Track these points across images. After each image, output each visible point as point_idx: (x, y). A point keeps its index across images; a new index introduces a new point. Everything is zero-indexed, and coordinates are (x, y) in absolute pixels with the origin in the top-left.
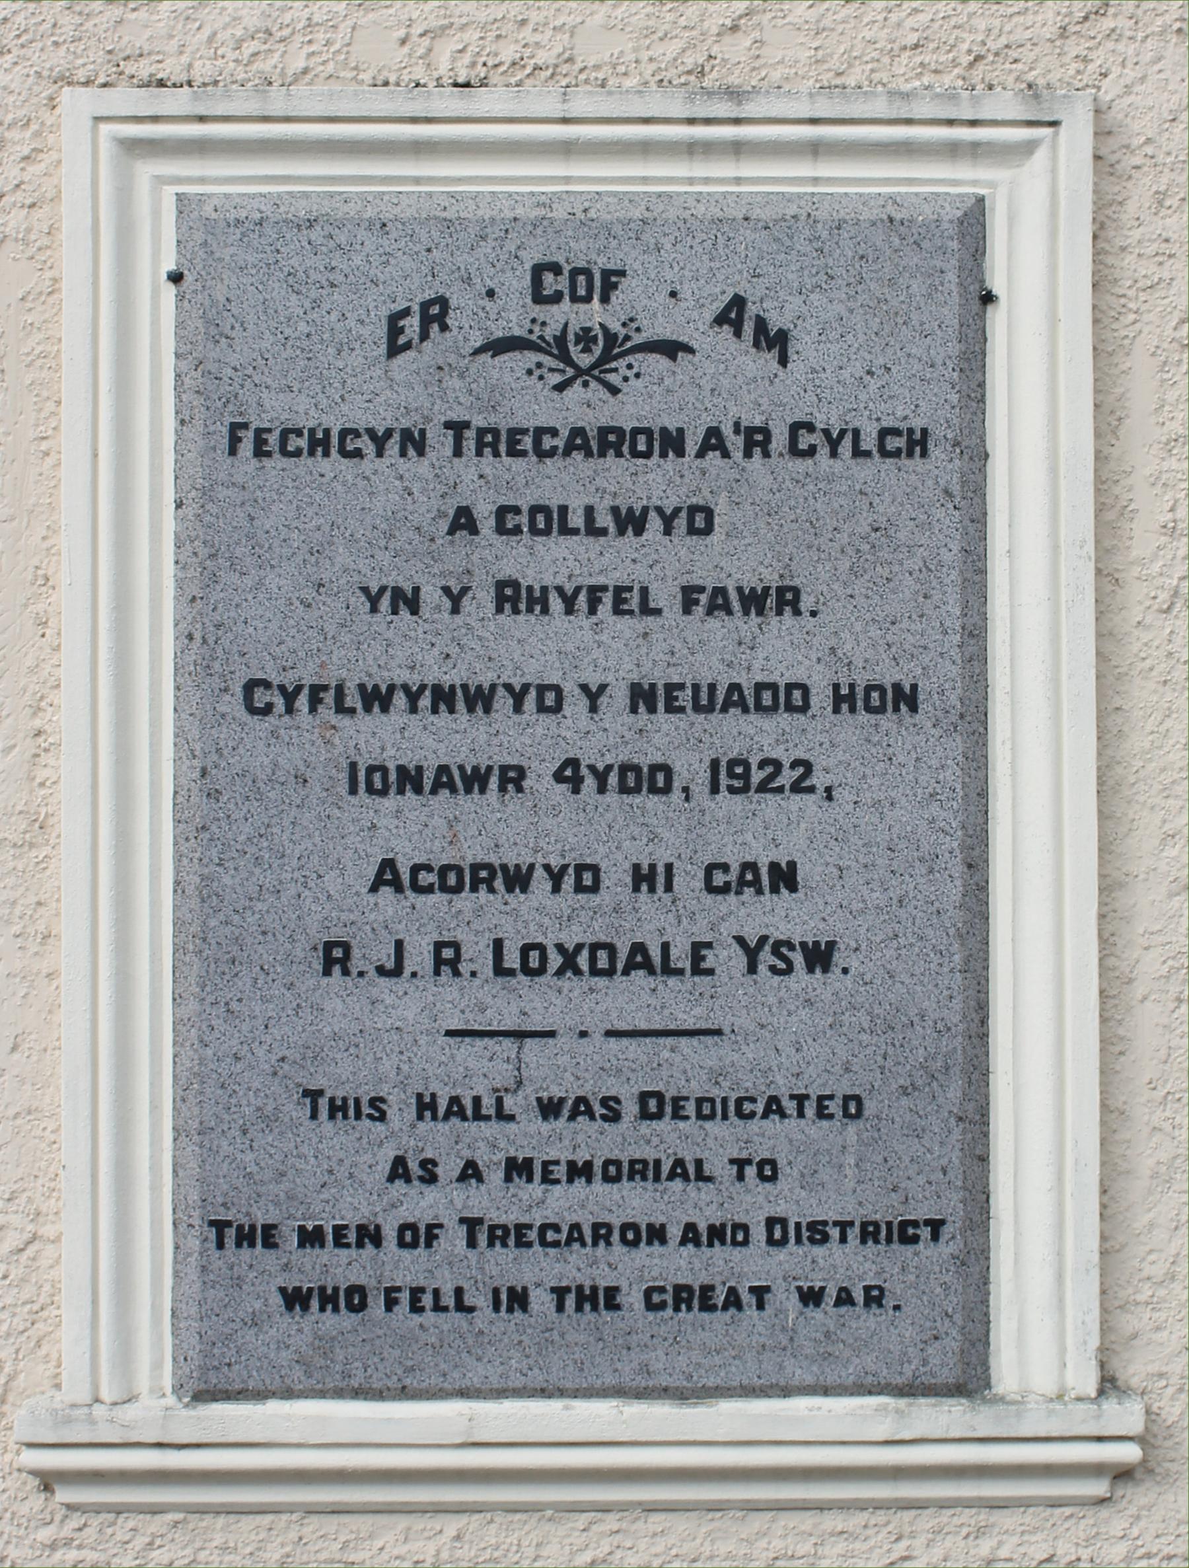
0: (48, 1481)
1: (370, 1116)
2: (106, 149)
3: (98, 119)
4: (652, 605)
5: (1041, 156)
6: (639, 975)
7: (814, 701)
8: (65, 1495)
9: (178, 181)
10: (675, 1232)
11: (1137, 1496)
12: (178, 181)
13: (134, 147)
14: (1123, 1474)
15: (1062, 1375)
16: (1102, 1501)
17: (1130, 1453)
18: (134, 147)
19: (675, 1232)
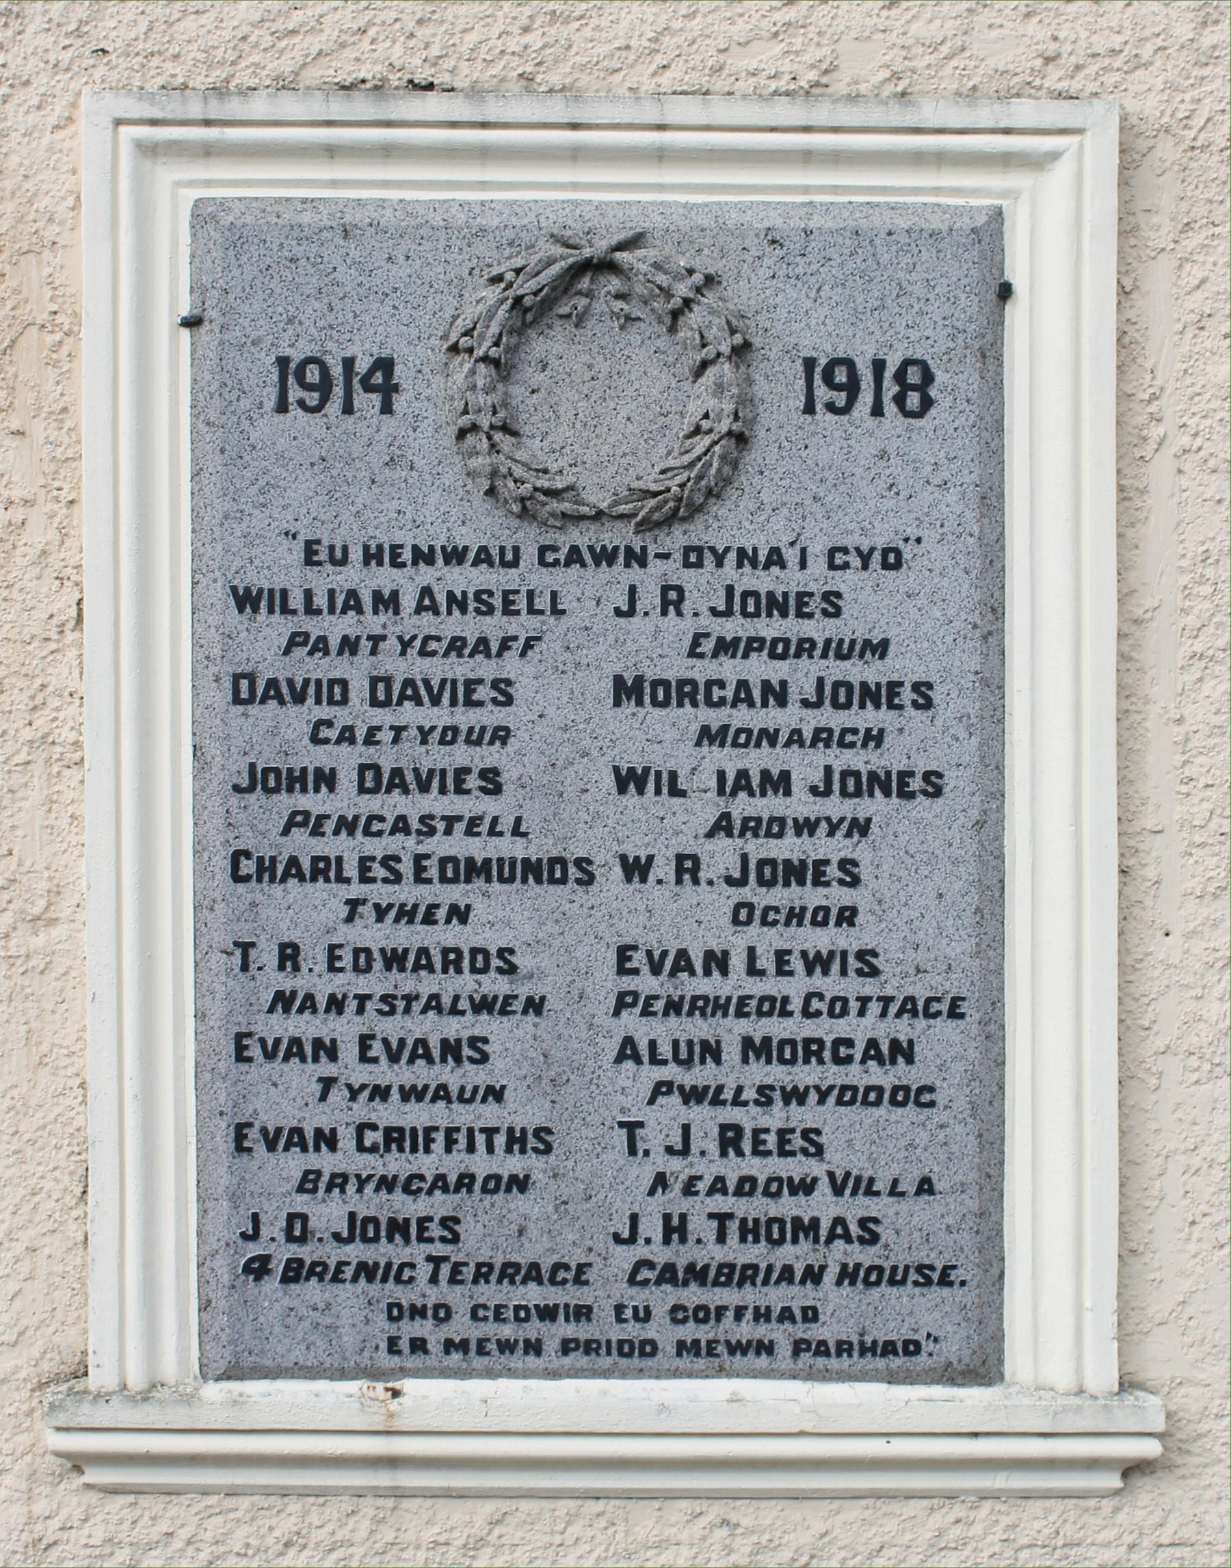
0: (77, 1463)
1: (535, 1150)
2: (126, 150)
3: (118, 122)
4: (560, 607)
5: (1061, 173)
6: (292, 882)
7: (352, 694)
8: (93, 1476)
9: (192, 184)
10: (395, 1095)
11: (1146, 1492)
12: (192, 184)
13: (148, 150)
14: (1133, 1469)
15: (1079, 1370)
16: (1117, 1492)
17: (1151, 1448)
18: (148, 150)
19: (395, 1095)
